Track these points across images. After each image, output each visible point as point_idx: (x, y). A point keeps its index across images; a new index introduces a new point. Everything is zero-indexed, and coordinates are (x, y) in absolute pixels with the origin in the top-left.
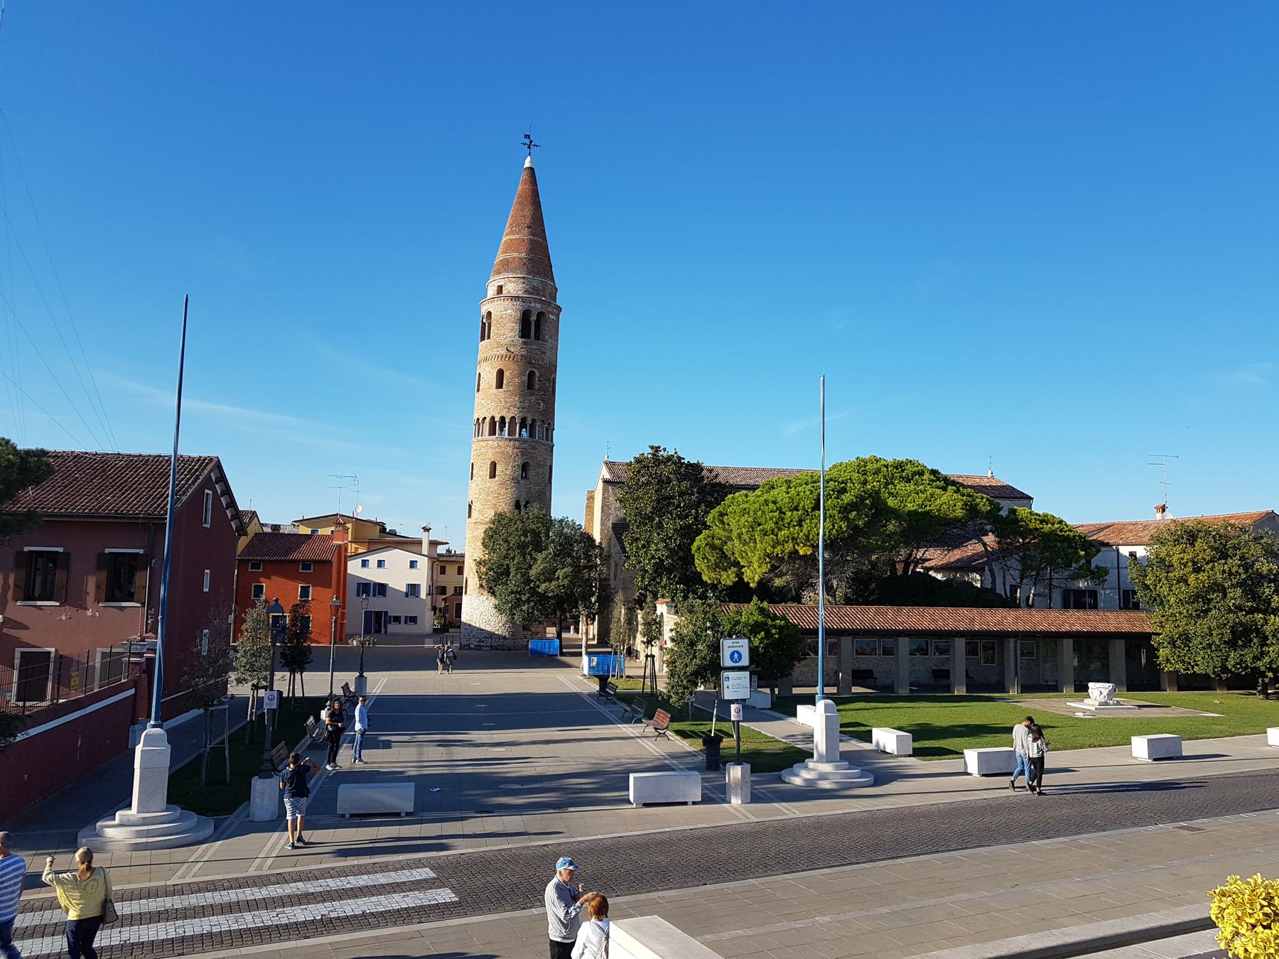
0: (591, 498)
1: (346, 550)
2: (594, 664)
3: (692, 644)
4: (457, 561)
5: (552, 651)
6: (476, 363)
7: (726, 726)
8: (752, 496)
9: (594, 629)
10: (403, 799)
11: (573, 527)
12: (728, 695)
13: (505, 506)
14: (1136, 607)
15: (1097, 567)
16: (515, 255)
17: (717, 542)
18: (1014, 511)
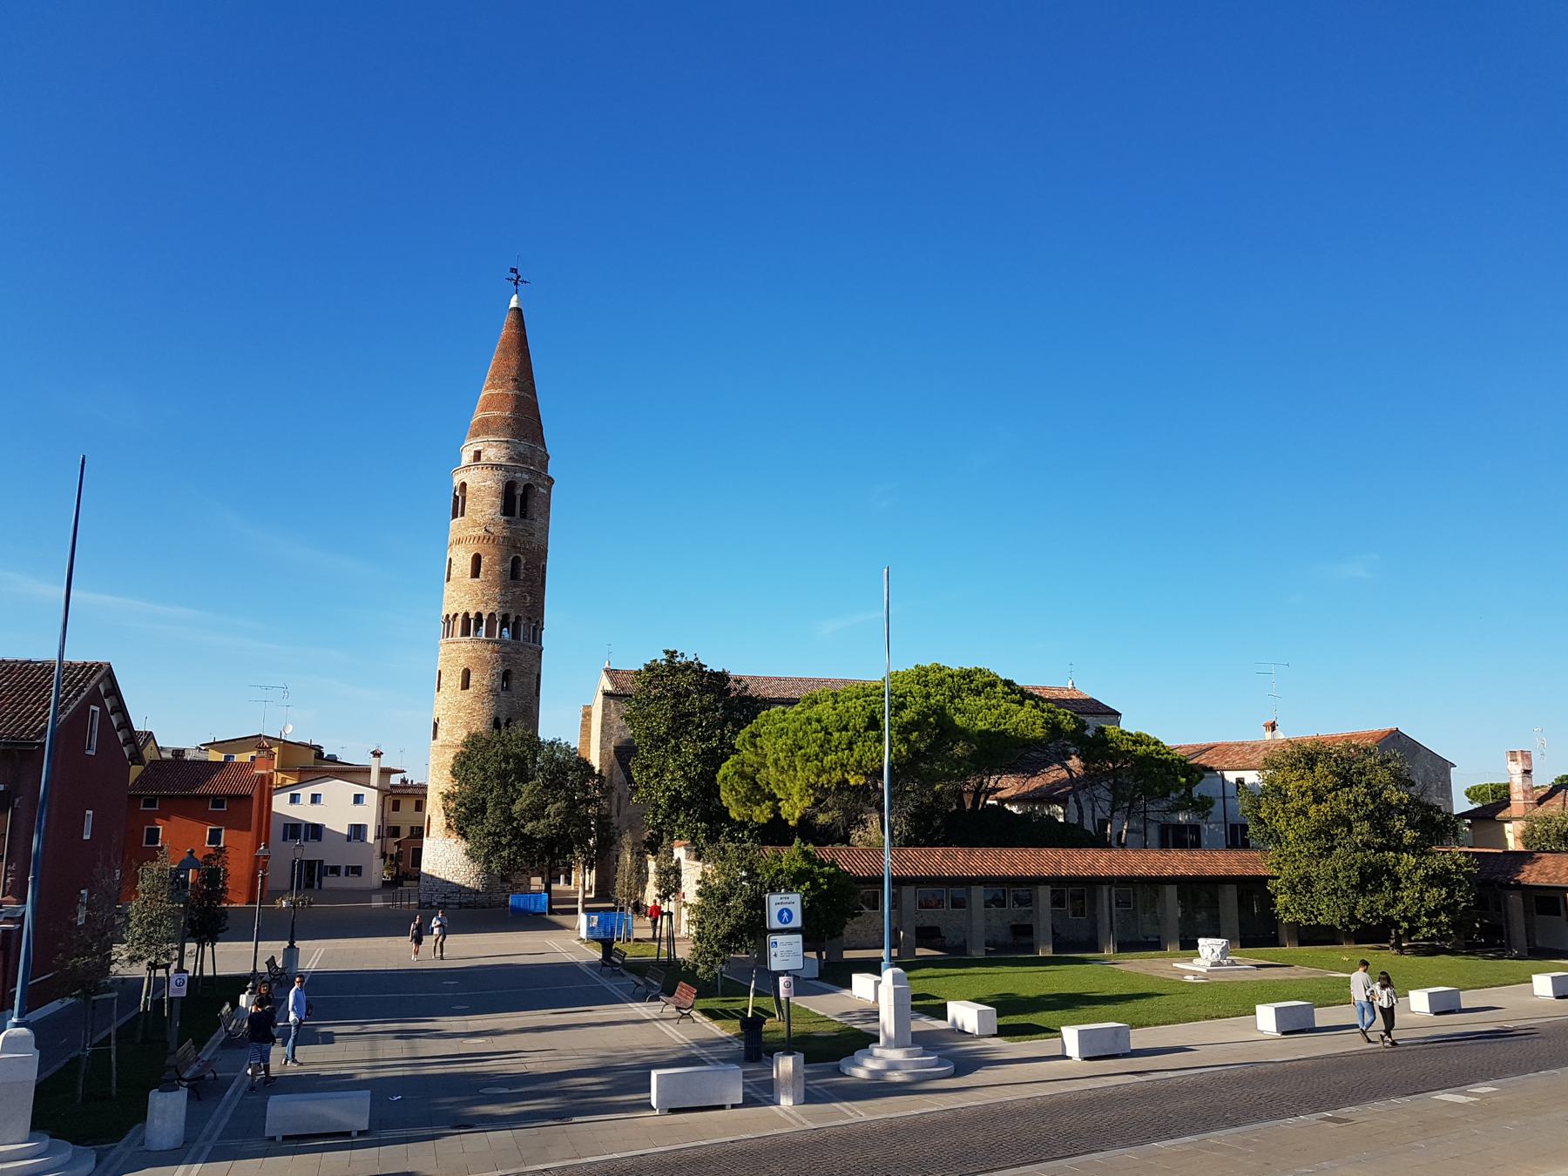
0: (587, 715)
1: (271, 781)
2: (595, 924)
3: (725, 899)
4: (418, 795)
5: (539, 909)
6: (445, 546)
7: (767, 1003)
8: (790, 712)
9: (591, 878)
10: (353, 1112)
11: (567, 750)
12: (776, 964)
13: (480, 725)
14: (1246, 845)
15: (1201, 797)
16: (497, 413)
17: (748, 770)
18: (1103, 730)
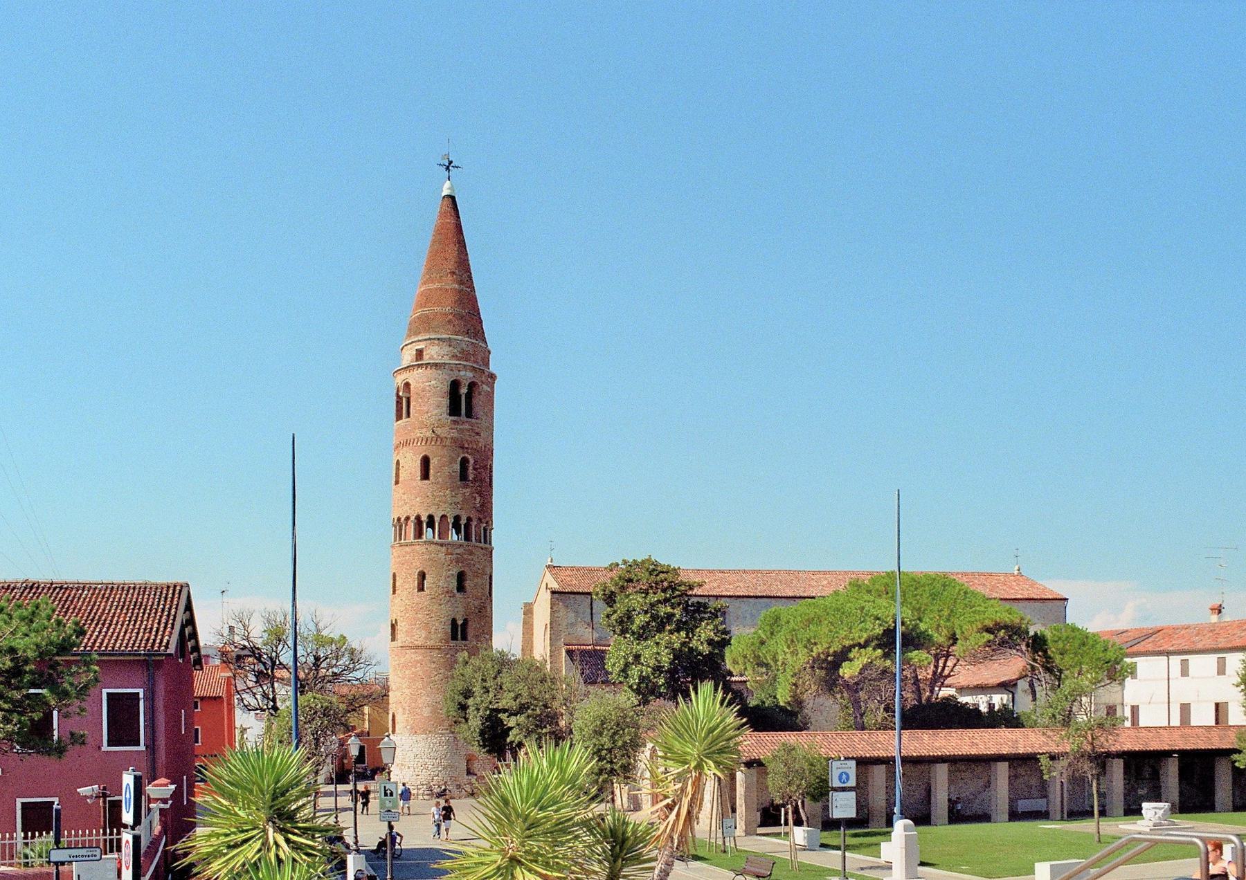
0: (528, 610)
